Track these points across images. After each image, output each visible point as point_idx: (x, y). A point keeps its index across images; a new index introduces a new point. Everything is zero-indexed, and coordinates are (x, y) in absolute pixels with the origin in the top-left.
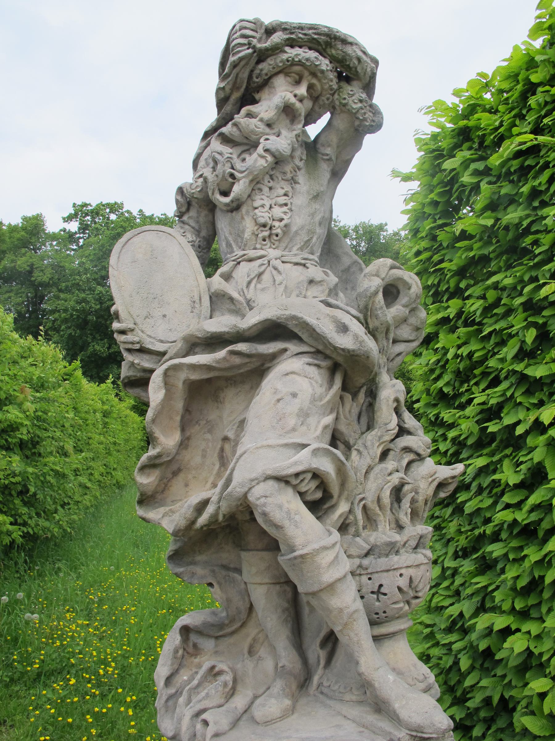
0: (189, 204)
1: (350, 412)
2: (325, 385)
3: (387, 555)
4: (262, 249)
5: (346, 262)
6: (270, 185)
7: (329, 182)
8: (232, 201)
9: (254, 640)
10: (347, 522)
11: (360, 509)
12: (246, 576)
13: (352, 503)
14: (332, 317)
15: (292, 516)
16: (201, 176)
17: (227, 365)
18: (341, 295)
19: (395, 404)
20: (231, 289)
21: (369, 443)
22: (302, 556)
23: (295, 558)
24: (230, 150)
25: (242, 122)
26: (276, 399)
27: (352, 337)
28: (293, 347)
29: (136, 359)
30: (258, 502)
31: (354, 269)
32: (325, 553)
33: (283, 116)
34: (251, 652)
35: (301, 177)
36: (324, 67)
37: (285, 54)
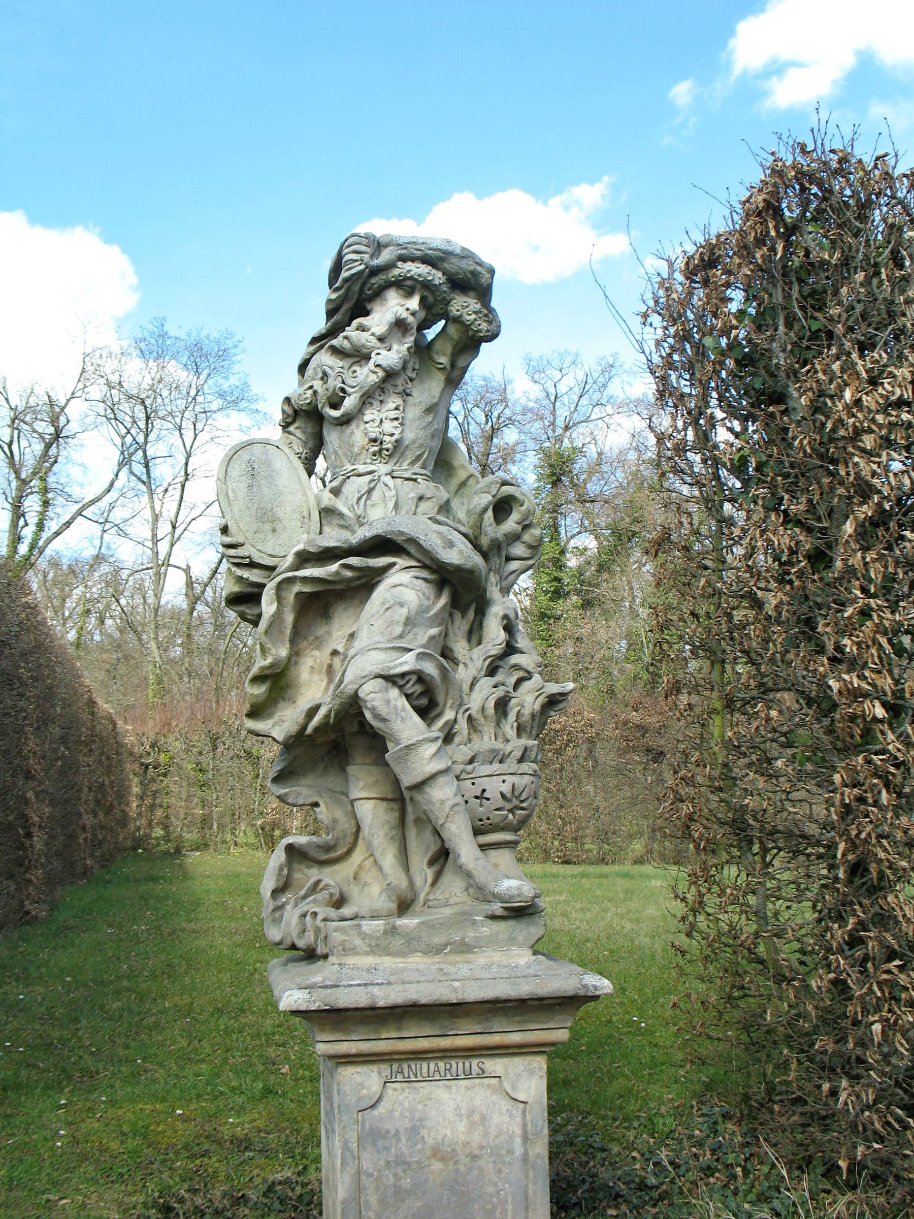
0: (296, 412)
8: (342, 416)
9: (360, 866)
16: (311, 387)
20: (341, 506)
24: (341, 364)
27: (458, 554)
28: (401, 562)
30: (368, 698)
33: (396, 329)
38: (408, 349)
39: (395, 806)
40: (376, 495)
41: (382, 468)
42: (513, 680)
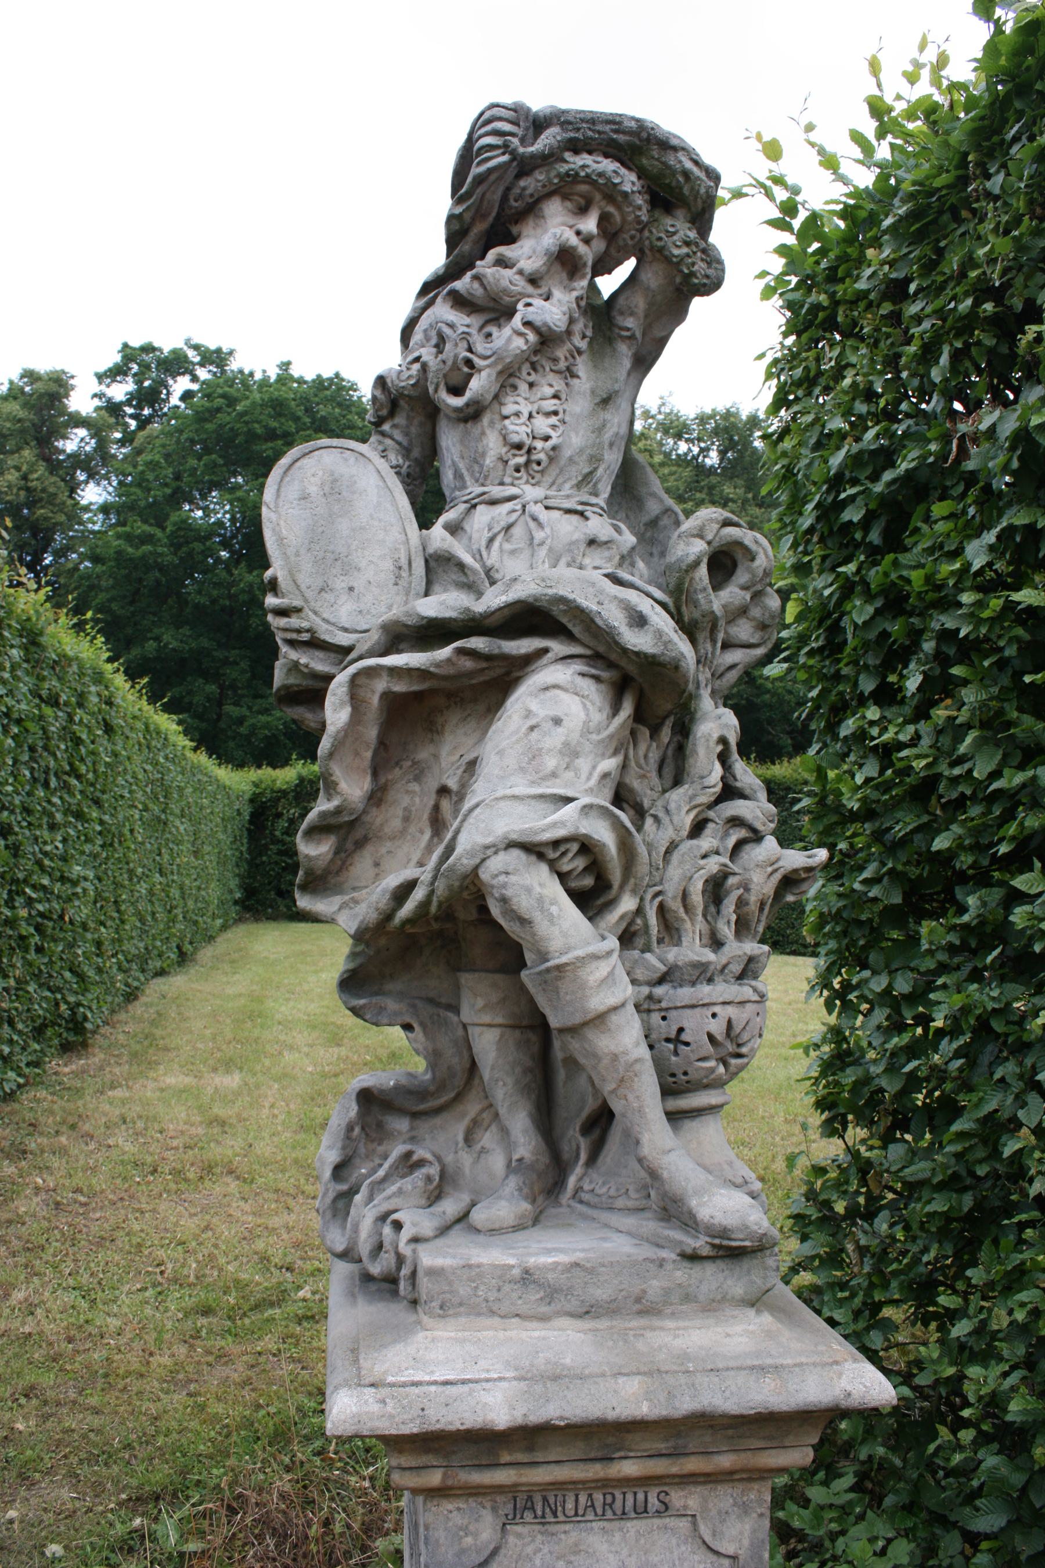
1: (646, 757)
2: (607, 710)
3: (693, 984)
5: (653, 508)
6: (531, 379)
7: (629, 374)
8: (467, 405)
10: (633, 928)
12: (467, 1014)
13: (642, 899)
14: (621, 601)
15: (546, 905)
16: (417, 359)
17: (451, 671)
18: (641, 564)
19: (720, 748)
21: (672, 806)
22: (559, 968)
23: (548, 970)
24: (467, 320)
27: (658, 634)
28: (557, 647)
29: (304, 658)
30: (495, 882)
31: (665, 521)
32: (595, 964)
33: (557, 267)
35: (582, 367)
36: (627, 188)
39: (533, 1037)
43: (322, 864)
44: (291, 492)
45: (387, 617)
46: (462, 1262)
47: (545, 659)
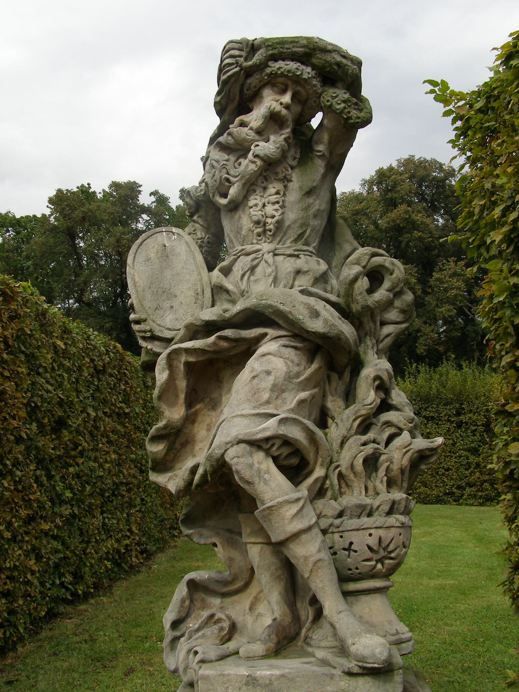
1: (336, 389)
4: (257, 243)
6: (264, 185)
11: (336, 475)
14: (305, 304)
17: (216, 348)
24: (226, 157)
25: (235, 132)
26: (252, 376)
27: (325, 320)
28: (271, 332)
34: (251, 608)
37: (269, 68)
38: (285, 139)
40: (259, 270)
41: (266, 247)
42: (386, 435)
43: (160, 456)
44: (141, 257)
45: (189, 319)
46: (219, 673)
47: (266, 340)
